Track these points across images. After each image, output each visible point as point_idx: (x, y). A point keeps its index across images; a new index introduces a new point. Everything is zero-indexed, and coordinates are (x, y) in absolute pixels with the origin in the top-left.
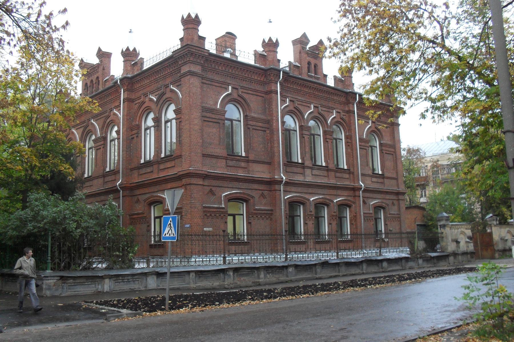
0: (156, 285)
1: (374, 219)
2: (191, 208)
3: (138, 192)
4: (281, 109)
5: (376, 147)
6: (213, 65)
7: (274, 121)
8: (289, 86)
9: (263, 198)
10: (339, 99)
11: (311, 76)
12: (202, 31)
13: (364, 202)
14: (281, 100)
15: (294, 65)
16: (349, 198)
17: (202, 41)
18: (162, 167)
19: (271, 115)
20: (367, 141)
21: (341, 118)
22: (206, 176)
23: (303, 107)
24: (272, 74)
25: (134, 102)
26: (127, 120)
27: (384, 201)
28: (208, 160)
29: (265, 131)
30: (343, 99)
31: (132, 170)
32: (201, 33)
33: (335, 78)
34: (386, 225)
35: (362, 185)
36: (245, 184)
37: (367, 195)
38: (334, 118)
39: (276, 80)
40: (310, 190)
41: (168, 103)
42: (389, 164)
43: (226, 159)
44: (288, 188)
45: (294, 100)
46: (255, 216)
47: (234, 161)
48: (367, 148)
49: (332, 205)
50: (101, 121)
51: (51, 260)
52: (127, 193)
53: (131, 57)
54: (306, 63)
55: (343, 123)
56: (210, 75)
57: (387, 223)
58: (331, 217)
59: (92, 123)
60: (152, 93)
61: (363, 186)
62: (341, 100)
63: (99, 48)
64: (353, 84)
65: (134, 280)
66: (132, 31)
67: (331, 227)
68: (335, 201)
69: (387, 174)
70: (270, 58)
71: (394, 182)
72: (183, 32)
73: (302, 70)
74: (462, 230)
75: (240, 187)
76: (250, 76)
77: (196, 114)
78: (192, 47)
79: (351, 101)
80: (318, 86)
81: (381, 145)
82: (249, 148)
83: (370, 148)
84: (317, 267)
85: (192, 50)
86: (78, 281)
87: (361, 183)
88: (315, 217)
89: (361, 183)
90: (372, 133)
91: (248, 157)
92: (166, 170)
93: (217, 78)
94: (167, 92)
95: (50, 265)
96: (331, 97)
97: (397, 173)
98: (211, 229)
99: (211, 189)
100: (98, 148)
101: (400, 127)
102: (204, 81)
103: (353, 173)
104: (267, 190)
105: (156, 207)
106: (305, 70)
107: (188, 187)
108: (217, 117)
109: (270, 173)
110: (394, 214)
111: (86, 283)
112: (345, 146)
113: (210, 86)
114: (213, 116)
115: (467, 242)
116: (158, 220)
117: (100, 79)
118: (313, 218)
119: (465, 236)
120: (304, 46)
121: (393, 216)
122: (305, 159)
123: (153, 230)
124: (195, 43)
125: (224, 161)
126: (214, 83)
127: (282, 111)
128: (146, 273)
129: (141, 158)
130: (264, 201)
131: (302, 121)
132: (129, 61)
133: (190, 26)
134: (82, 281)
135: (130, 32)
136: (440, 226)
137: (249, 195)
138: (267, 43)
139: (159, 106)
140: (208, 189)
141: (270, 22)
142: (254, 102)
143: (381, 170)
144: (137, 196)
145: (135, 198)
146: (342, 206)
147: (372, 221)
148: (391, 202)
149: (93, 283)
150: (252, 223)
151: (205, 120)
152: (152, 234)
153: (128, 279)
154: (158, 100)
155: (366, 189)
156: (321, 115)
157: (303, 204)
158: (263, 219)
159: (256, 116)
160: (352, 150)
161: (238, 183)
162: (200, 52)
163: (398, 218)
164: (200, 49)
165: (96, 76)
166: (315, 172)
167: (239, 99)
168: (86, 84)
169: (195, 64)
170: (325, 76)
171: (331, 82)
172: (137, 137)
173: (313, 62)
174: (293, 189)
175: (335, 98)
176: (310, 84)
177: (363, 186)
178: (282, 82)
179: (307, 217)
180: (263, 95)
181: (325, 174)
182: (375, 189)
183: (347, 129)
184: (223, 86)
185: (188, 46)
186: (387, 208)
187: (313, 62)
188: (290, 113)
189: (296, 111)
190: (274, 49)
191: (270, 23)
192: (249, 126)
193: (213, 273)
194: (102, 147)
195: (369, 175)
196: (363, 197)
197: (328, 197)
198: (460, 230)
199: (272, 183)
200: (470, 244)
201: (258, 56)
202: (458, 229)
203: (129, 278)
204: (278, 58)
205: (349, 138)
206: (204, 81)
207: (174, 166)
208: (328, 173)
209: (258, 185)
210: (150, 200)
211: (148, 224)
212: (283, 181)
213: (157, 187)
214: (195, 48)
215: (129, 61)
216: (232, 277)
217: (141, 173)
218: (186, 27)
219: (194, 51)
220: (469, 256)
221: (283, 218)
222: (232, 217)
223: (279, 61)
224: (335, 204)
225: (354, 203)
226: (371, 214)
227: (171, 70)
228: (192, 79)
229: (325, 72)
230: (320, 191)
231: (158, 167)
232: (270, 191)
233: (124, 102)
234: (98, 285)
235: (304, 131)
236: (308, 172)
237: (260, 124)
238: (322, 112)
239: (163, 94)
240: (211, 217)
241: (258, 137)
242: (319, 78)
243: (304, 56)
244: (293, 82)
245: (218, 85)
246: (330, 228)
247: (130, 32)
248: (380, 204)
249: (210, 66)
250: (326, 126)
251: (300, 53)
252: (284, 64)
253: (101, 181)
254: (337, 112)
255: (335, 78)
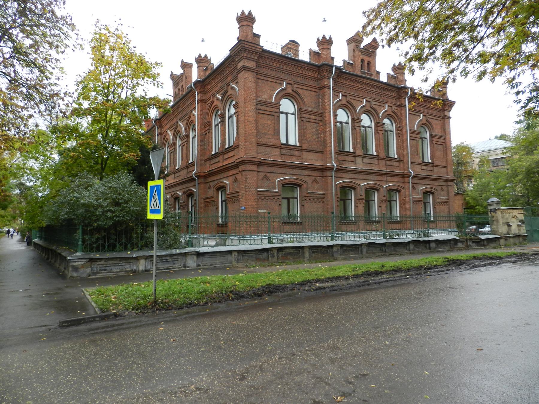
0: (196, 264)
1: (423, 203)
2: (246, 192)
3: (210, 179)
4: (333, 103)
5: (426, 138)
6: (268, 62)
7: (327, 114)
8: (342, 82)
9: (315, 183)
10: (391, 94)
11: (365, 73)
12: (257, 29)
13: (413, 187)
14: (334, 95)
15: (348, 63)
16: (399, 184)
17: (257, 39)
18: (226, 156)
19: (324, 108)
20: (418, 133)
21: (392, 112)
22: (260, 164)
23: (355, 101)
24: (325, 69)
25: (206, 103)
26: (201, 118)
27: (434, 187)
28: (262, 149)
29: (319, 123)
30: (394, 94)
31: (206, 161)
32: (255, 31)
33: (388, 75)
34: (434, 208)
35: (411, 172)
36: (298, 170)
37: (416, 181)
38: (386, 111)
39: (329, 75)
40: (361, 177)
41: (230, 100)
42: (439, 154)
43: (280, 148)
44: (340, 175)
45: (347, 94)
46: (308, 199)
47: (288, 150)
48: (418, 139)
49: (382, 190)
50: (185, 122)
51: (82, 242)
52: (202, 180)
53: (202, 63)
54: (360, 61)
55: (395, 116)
56: (264, 71)
57: (435, 207)
58: (381, 201)
59: (179, 124)
60: (218, 92)
61: (412, 173)
62: (393, 95)
63: (182, 60)
64: (406, 80)
65: (173, 260)
66: (204, 40)
67: (381, 209)
68: (385, 186)
69: (436, 163)
70: (324, 55)
71: (444, 170)
72: (238, 30)
73: (355, 67)
74: (514, 214)
75: (293, 173)
76: (304, 73)
77: (251, 107)
78: (246, 43)
79: (402, 96)
80: (371, 82)
81: (431, 136)
82: (302, 138)
83: (420, 140)
84: (363, 247)
85: (245, 46)
86: (111, 262)
87: (410, 170)
88: (365, 201)
89: (410, 170)
90: (423, 126)
91: (301, 147)
92: (229, 159)
93: (273, 73)
94: (229, 90)
95: (80, 247)
96: (383, 92)
97: (447, 161)
98: (265, 211)
99: (265, 175)
100: (184, 144)
101: (451, 120)
102: (259, 77)
103: (403, 161)
104: (320, 177)
105: (223, 193)
106: (358, 67)
107: (243, 173)
108: (272, 110)
109: (323, 161)
110: (443, 199)
111: (120, 264)
112: (396, 137)
113: (265, 81)
114: (268, 109)
115: (518, 225)
116: (224, 203)
117: (184, 87)
118: (364, 201)
119: (517, 220)
120: (358, 44)
121: (441, 200)
122: (357, 148)
123: (220, 211)
124: (250, 39)
125: (279, 150)
126: (268, 79)
127: (334, 105)
128: (185, 253)
129: (212, 151)
130: (316, 186)
131: (354, 114)
132: (202, 66)
133: (245, 23)
134: (115, 262)
135: (202, 41)
136: (491, 210)
137: (302, 180)
138: (321, 41)
139: (223, 103)
140: (263, 174)
141: (325, 21)
142: (309, 97)
143: (431, 159)
144: (209, 184)
145: (208, 185)
146: (392, 191)
147: (421, 204)
148: (440, 187)
149: (127, 264)
150: (305, 205)
151: (258, 112)
152: (220, 214)
153: (166, 260)
154: (223, 97)
155: (416, 176)
156: (373, 109)
157: (354, 189)
158: (315, 202)
159: (310, 109)
160: (403, 141)
161: (291, 170)
162: (253, 48)
163: (447, 202)
164: (256, 46)
165: (181, 85)
166: (366, 160)
167: (293, 93)
168: (176, 92)
169: (250, 60)
170: (378, 73)
171: (383, 78)
172: (209, 132)
173: (366, 59)
174: (344, 175)
175: (387, 93)
176: (363, 79)
177: (412, 173)
178: (335, 77)
179: (357, 201)
180: (317, 90)
181: (376, 161)
182: (424, 176)
183: (398, 121)
184: (278, 81)
185: (242, 42)
186: (436, 194)
187: (366, 59)
188: (343, 107)
189: (348, 105)
190: (328, 47)
191: (325, 22)
192: (303, 119)
193: (257, 252)
194: (185, 143)
195: (418, 164)
196: (412, 183)
197: (378, 183)
198: (511, 214)
199: (324, 170)
200: (522, 228)
201: (313, 54)
202: (510, 213)
203: (168, 258)
204: (332, 55)
205: (400, 129)
206: (259, 77)
207: (234, 156)
208: (379, 162)
209: (311, 171)
210: (217, 185)
211: (216, 207)
212: (334, 168)
213: (223, 174)
214: (248, 44)
215: (202, 66)
216: (276, 257)
217: (212, 163)
218: (241, 24)
219: (247, 46)
220: (521, 239)
221: (334, 201)
222: (286, 201)
223: (333, 59)
224: (385, 189)
225: (404, 188)
226: (420, 198)
227: (231, 69)
228: (247, 74)
229: (378, 69)
230: (370, 177)
231: (223, 157)
232: (322, 177)
233: (198, 103)
234: (133, 265)
235: (356, 123)
236: (359, 160)
237: (314, 117)
238: (374, 106)
239: (226, 92)
240: (265, 200)
241: (311, 128)
242: (372, 74)
243: (358, 53)
244: (346, 78)
245: (272, 80)
246: (380, 210)
247: (202, 41)
248: (429, 189)
249: (264, 62)
250: (377, 119)
251: (354, 51)
252: (338, 62)
253: (185, 171)
254: (389, 106)
255: (388, 75)
